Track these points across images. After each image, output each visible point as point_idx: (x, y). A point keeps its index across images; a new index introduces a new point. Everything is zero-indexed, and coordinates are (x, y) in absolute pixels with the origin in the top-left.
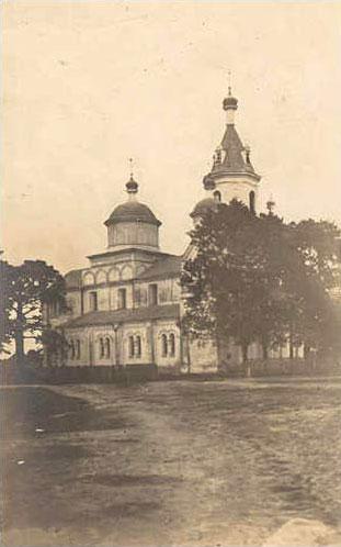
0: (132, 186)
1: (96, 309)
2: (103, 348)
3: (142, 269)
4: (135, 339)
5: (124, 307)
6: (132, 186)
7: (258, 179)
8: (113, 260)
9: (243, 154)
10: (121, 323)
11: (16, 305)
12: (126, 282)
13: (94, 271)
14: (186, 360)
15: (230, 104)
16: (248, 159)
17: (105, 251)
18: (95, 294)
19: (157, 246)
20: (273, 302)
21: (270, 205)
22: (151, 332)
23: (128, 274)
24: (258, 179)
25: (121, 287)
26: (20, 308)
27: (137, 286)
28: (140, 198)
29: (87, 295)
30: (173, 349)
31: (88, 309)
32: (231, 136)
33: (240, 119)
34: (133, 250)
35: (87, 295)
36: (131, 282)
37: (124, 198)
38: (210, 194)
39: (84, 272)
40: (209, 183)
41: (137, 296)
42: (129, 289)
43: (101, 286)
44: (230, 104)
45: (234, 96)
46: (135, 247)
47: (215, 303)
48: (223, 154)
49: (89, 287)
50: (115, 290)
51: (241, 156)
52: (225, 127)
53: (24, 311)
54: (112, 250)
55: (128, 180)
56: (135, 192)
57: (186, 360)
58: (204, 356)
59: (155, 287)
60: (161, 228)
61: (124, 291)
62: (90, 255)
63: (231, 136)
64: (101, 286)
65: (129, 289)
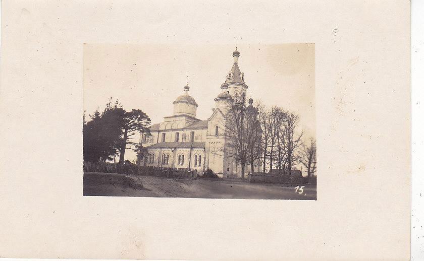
1: (164, 141)
2: (196, 160)
4: (198, 158)
5: (178, 141)
6: (187, 88)
8: (175, 119)
9: (241, 75)
12: (179, 130)
15: (236, 54)
16: (243, 78)
18: (164, 134)
24: (247, 87)
27: (185, 132)
30: (200, 163)
31: (160, 141)
34: (185, 116)
36: (182, 129)
37: (183, 93)
40: (225, 86)
41: (184, 137)
43: (168, 130)
44: (236, 54)
45: (238, 50)
48: (232, 75)
50: (174, 133)
59: (193, 133)
61: (178, 134)
63: (236, 64)
64: (168, 130)
65: (181, 133)
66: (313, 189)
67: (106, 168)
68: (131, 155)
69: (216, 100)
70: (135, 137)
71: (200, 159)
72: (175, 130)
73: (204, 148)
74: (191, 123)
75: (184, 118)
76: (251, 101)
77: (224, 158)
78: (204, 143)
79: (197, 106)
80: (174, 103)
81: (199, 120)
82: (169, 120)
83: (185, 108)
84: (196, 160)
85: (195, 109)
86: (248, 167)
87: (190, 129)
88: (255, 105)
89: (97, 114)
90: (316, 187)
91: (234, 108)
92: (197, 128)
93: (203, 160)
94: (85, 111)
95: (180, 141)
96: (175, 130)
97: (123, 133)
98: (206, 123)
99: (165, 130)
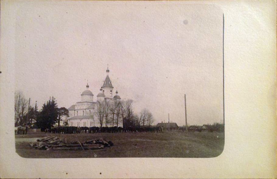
0: (88, 86)
5: (84, 115)
6: (88, 86)
10: (82, 119)
11: (59, 116)
12: (84, 109)
15: (108, 71)
18: (78, 112)
19: (93, 101)
20: (108, 120)
21: (117, 92)
22: (87, 121)
23: (85, 108)
25: (83, 110)
29: (76, 112)
31: (76, 115)
33: (110, 75)
34: (86, 102)
35: (76, 112)
36: (85, 109)
37: (85, 89)
38: (102, 92)
43: (79, 110)
44: (108, 71)
45: (109, 69)
47: (36, 123)
48: (105, 82)
49: (77, 110)
50: (82, 111)
51: (109, 83)
53: (60, 117)
54: (82, 101)
58: (32, 116)
59: (90, 111)
60: (94, 96)
61: (84, 111)
64: (79, 110)
65: (85, 111)
66: (22, 140)
68: (62, 124)
69: (98, 96)
70: (63, 118)
72: (82, 109)
74: (89, 105)
79: (93, 95)
82: (79, 104)
83: (87, 98)
85: (93, 97)
87: (88, 109)
89: (44, 105)
90: (15, 141)
94: (36, 101)
95: (85, 115)
96: (82, 109)
97: (58, 120)
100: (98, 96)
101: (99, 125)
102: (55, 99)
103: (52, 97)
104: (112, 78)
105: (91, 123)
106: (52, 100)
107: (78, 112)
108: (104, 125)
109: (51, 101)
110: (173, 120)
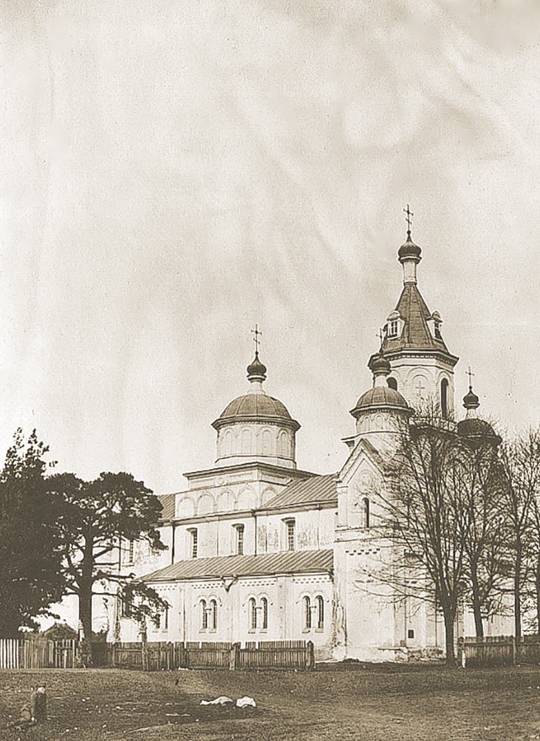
0: (257, 371)
2: (309, 613)
3: (271, 495)
6: (257, 371)
7: (453, 361)
8: (226, 478)
9: (431, 324)
11: (83, 543)
12: (241, 514)
13: (195, 495)
14: (341, 637)
15: (410, 253)
16: (437, 333)
17: (213, 466)
24: (453, 361)
26: (90, 545)
28: (272, 387)
30: (321, 619)
32: (411, 294)
34: (260, 466)
36: (254, 513)
39: (178, 498)
40: (379, 365)
42: (248, 522)
44: (410, 253)
45: (416, 242)
46: (260, 460)
49: (186, 521)
52: (71, 473)
53: (96, 551)
55: (250, 361)
56: (262, 380)
57: (341, 637)
59: (291, 523)
62: (350, 410)
67: (98, 519)
69: (356, 413)
71: (321, 607)
73: (331, 573)
75: (255, 474)
76: (471, 401)
77: (486, 423)
78: (329, 554)
79: (295, 426)
80: (217, 425)
81: (305, 476)
84: (309, 613)
86: (467, 625)
88: (482, 413)
91: (416, 432)
92: (301, 507)
93: (328, 608)
98: (335, 479)
99: (197, 519)
100: (356, 413)
101: (514, 618)
102: (46, 450)
103: (27, 434)
104: (431, 294)
105: (314, 602)
106: (29, 453)
107: (195, 533)
108: (514, 614)
109: (21, 453)
110: (148, 638)
